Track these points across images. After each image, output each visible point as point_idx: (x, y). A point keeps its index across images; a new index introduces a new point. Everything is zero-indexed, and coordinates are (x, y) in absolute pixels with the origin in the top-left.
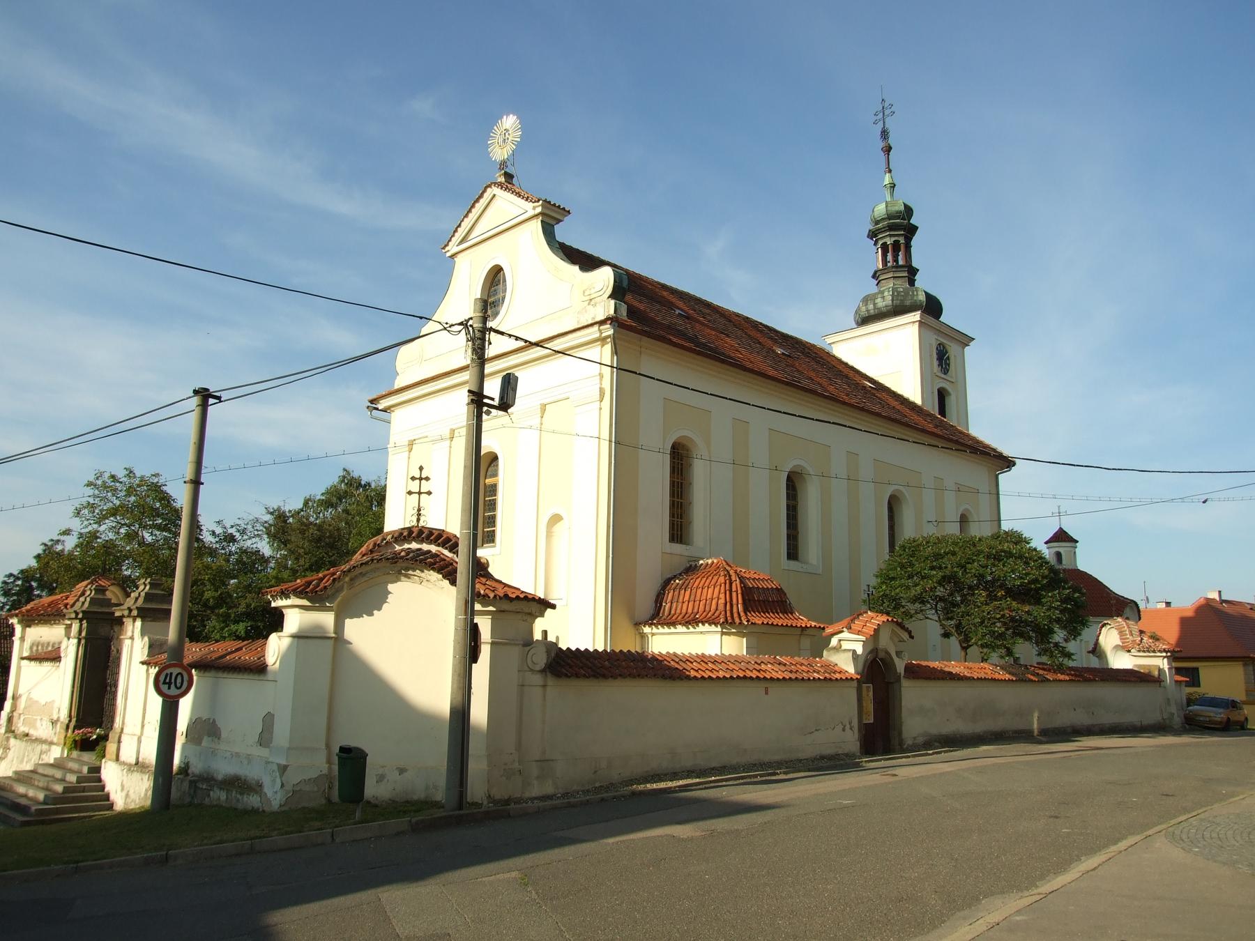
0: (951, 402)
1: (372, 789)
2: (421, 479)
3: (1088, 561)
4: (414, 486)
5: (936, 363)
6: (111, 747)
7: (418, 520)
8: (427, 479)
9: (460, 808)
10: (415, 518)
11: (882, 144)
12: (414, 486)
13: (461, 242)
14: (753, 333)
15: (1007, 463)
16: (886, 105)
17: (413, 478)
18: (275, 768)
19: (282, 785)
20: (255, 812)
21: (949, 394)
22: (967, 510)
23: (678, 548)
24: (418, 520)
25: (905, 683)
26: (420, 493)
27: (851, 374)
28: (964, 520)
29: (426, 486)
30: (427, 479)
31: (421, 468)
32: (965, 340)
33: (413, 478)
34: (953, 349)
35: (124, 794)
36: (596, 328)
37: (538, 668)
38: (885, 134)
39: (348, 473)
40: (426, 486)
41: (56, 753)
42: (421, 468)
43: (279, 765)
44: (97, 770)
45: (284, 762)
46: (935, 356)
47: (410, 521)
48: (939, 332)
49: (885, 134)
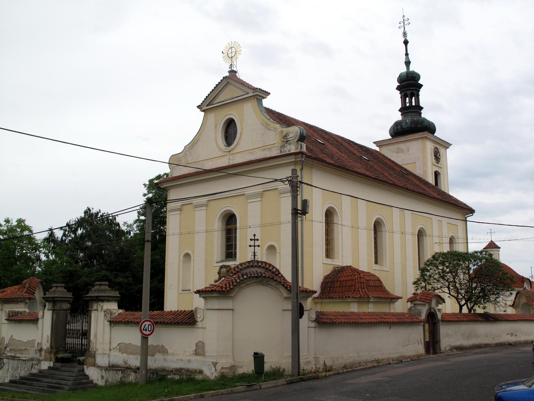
0: (442, 178)
1: (267, 367)
2: (254, 240)
3: (506, 257)
4: (252, 243)
5: (434, 158)
6: (90, 360)
7: (254, 258)
8: (257, 240)
9: (299, 375)
10: (253, 257)
11: (403, 40)
12: (252, 243)
13: (207, 106)
14: (347, 146)
15: (471, 211)
16: (405, 19)
17: (251, 240)
18: (211, 364)
19: (216, 370)
20: (203, 381)
21: (440, 174)
22: (452, 236)
23: (329, 261)
24: (254, 258)
25: (441, 323)
26: (254, 246)
27: (389, 162)
28: (452, 241)
29: (257, 243)
30: (257, 240)
31: (255, 235)
32: (447, 145)
33: (251, 240)
34: (442, 150)
35: (104, 381)
36: (293, 157)
37: (313, 320)
38: (405, 34)
39: (90, 210)
40: (257, 243)
41: (45, 365)
42: (255, 235)
43: (213, 363)
44: (83, 370)
45: (215, 361)
46: (433, 155)
47: (250, 258)
48: (435, 142)
49: (405, 34)
